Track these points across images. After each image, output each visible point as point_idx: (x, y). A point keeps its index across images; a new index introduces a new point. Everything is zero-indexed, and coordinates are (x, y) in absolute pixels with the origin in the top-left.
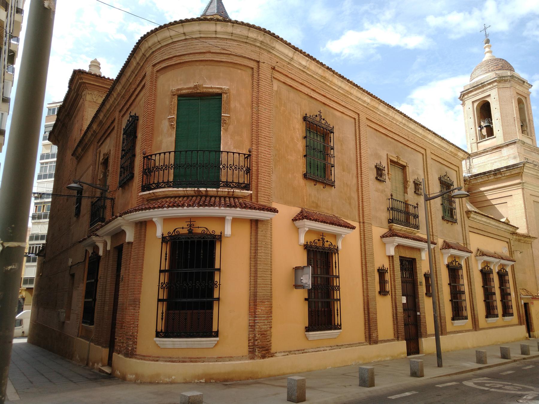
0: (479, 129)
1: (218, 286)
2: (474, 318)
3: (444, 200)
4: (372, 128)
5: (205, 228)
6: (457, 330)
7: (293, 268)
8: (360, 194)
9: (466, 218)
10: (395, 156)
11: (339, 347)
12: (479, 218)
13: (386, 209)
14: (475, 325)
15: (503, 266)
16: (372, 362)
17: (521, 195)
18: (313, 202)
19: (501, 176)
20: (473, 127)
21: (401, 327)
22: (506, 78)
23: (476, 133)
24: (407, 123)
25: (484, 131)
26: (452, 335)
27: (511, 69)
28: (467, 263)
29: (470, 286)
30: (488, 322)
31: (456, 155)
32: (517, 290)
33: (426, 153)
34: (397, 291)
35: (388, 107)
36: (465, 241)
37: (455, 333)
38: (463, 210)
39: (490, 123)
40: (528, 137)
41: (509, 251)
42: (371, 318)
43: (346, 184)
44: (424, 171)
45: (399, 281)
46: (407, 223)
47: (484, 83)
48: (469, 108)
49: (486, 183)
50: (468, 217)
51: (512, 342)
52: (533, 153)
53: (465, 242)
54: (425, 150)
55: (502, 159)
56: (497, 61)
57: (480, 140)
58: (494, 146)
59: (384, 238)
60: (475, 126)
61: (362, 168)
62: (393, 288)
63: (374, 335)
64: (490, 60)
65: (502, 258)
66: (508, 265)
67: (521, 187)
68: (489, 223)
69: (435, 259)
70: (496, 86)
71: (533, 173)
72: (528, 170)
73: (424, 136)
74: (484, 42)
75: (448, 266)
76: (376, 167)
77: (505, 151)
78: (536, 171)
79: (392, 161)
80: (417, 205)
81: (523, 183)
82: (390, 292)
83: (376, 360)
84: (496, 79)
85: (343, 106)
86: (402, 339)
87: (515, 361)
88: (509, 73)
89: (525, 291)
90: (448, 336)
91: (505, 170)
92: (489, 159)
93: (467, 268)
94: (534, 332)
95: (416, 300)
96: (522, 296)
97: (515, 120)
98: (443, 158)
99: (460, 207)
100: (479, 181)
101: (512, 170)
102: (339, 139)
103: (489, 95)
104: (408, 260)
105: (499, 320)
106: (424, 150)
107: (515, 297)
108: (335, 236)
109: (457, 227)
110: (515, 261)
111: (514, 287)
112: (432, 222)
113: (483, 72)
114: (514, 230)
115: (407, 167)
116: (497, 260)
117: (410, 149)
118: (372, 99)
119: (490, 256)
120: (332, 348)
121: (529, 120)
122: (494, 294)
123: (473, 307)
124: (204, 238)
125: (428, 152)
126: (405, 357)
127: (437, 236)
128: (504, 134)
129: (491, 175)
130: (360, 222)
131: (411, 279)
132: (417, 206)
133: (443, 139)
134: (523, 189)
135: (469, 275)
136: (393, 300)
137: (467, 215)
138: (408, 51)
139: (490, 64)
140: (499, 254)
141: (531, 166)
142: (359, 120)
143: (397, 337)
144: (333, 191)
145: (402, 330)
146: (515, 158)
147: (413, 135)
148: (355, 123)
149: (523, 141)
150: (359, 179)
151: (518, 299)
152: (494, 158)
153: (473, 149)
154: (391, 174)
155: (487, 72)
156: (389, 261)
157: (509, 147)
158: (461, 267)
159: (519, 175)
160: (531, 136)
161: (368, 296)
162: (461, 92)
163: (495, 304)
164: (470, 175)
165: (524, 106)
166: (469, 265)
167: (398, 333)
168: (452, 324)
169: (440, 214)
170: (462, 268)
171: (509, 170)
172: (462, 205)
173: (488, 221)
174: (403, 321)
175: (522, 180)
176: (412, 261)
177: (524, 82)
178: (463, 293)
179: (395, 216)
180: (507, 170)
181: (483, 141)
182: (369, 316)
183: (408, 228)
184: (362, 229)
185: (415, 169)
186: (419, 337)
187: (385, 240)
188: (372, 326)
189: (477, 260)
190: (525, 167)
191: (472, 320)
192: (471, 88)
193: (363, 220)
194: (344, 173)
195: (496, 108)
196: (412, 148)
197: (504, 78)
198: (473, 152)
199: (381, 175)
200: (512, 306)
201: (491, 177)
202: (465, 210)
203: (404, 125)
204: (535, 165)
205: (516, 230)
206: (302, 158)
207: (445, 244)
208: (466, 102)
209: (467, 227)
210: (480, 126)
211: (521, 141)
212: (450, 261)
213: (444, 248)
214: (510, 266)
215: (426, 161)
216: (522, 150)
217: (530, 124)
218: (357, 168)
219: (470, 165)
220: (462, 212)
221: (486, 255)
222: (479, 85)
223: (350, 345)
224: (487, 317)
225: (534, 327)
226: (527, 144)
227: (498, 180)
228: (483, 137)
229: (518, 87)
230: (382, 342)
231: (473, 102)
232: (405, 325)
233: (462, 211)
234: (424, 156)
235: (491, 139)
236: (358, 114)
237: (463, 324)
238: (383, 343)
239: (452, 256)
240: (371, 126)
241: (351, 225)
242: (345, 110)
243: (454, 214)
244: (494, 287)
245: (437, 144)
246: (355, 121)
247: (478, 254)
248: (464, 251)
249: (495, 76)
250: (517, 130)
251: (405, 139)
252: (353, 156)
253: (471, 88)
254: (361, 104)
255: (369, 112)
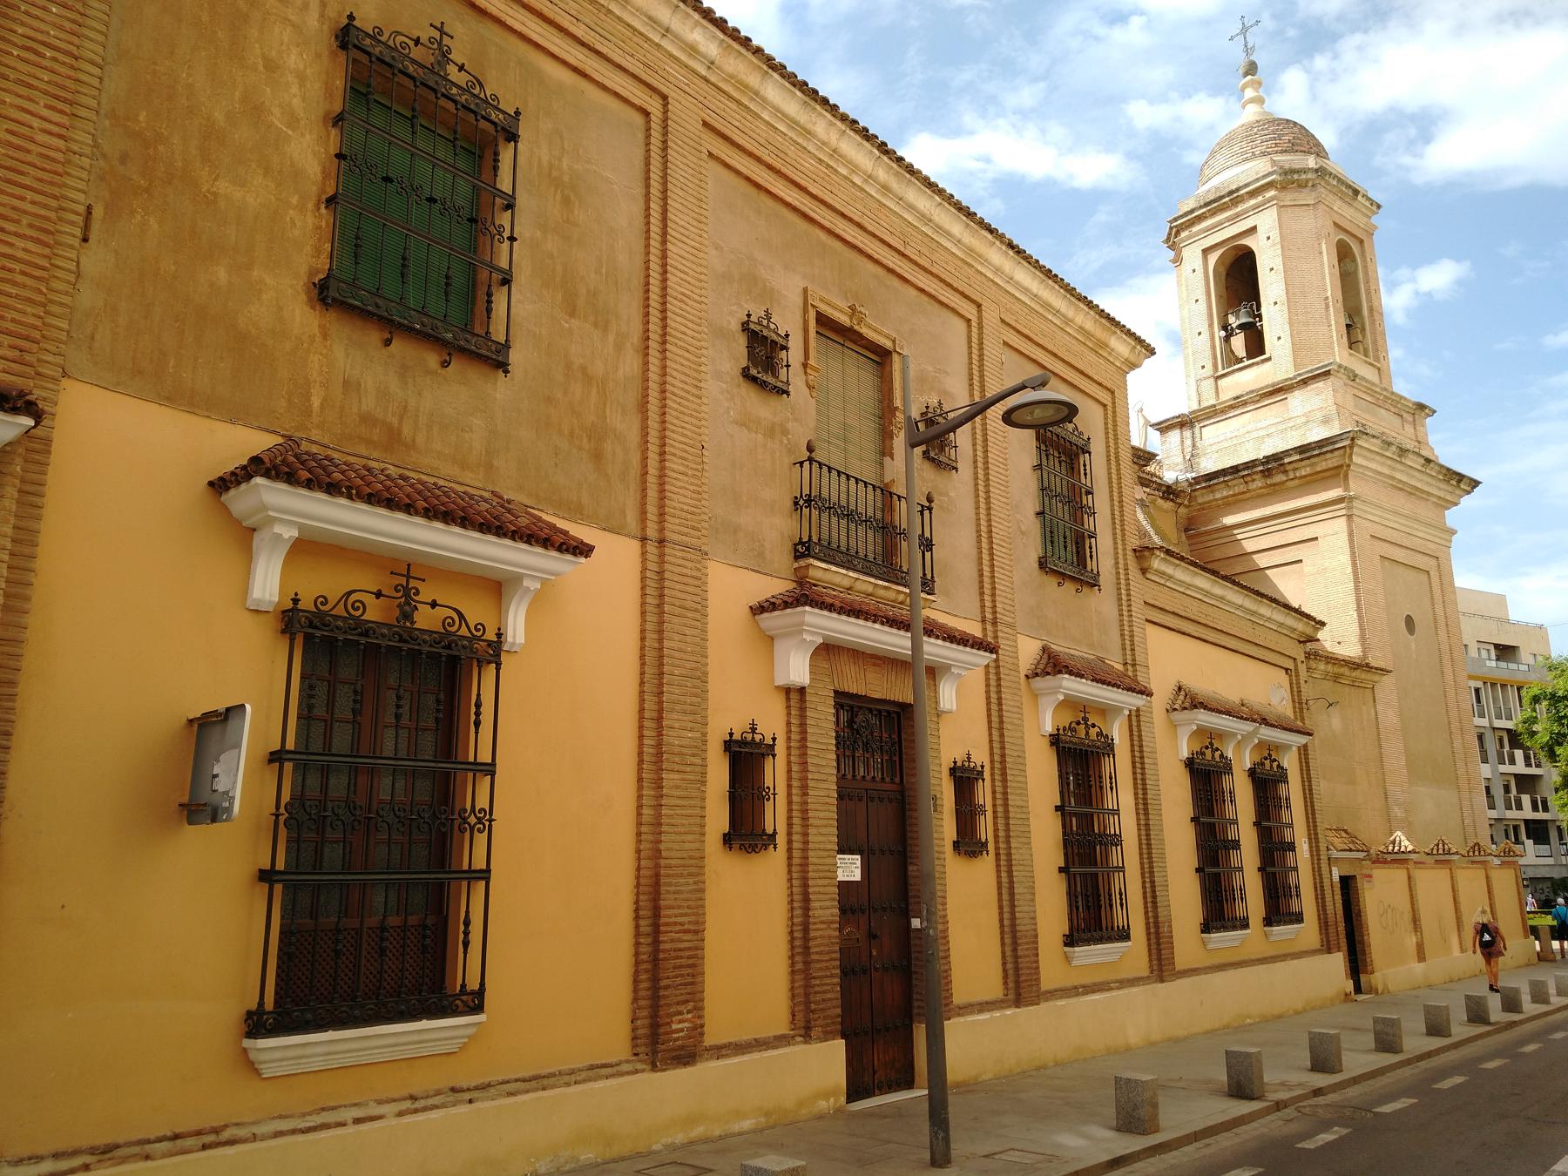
0: (1223, 333)
1: (772, 796)
2: (1157, 933)
3: (1050, 499)
4: (738, 173)
5: (455, 610)
6: (1088, 980)
7: (191, 721)
8: (653, 423)
9: (1134, 572)
10: (844, 305)
11: (467, 1096)
12: (1182, 574)
13: (789, 504)
14: (1159, 959)
15: (1269, 751)
16: (655, 1147)
17: (1345, 537)
18: (367, 419)
19: (1284, 478)
20: (1204, 328)
21: (828, 981)
22: (1304, 176)
23: (1213, 347)
24: (894, 184)
25: (1238, 343)
26: (1060, 1003)
27: (1317, 149)
28: (1135, 733)
29: (1142, 817)
30: (1210, 946)
31: (1104, 345)
32: (1316, 834)
33: (980, 318)
34: (811, 831)
35: (807, 99)
36: (1128, 652)
37: (1077, 995)
38: (1124, 545)
39: (1255, 317)
40: (1366, 362)
41: (1293, 701)
42: (665, 951)
43: (583, 369)
44: (971, 385)
45: (824, 788)
46: (887, 566)
47: (1238, 190)
48: (1194, 271)
49: (1240, 501)
50: (1144, 571)
51: (1297, 1013)
52: (1383, 411)
53: (1129, 657)
54: (979, 306)
55: (1290, 425)
56: (1278, 125)
57: (1223, 369)
58: (1266, 387)
59: (766, 615)
60: (1211, 326)
61: (669, 314)
62: (796, 821)
63: (674, 1026)
64: (1257, 122)
65: (1264, 721)
66: (1288, 747)
67: (1343, 512)
68: (1222, 598)
69: (1001, 710)
70: (1272, 199)
71: (1380, 469)
72: (1365, 458)
73: (970, 250)
74: (1241, 71)
75: (1055, 740)
76: (745, 327)
77: (1298, 402)
78: (1389, 462)
79: (822, 320)
80: (930, 500)
81: (1351, 499)
82: (991, 846)
83: (680, 1138)
84: (1274, 176)
85: (583, 44)
86: (826, 1033)
87: (1279, 1106)
88: (1311, 162)
89: (1344, 835)
90: (1044, 1006)
91: (1297, 457)
92: (1249, 428)
93: (1133, 751)
94: (1373, 972)
95: (911, 868)
96: (1335, 854)
97: (1327, 306)
98: (1050, 347)
99: (1114, 534)
100: (1218, 495)
101: (1316, 460)
102: (555, 174)
103: (1253, 230)
104: (880, 711)
105: (1253, 937)
106: (974, 307)
107: (1312, 856)
108: (497, 587)
109: (1102, 603)
110: (1310, 735)
111: (1308, 822)
112: (993, 571)
113: (1235, 160)
114: (1309, 631)
115: (895, 357)
116: (1248, 727)
117: (914, 293)
118: (730, 46)
119: (1220, 712)
120: (418, 1105)
121: (1371, 309)
122: (1236, 845)
123: (1154, 891)
124: (449, 647)
125: (991, 316)
126: (839, 1110)
127: (1011, 626)
128: (1296, 349)
129: (1254, 477)
130: (644, 539)
131: (888, 787)
132: (927, 504)
133: (1048, 273)
134: (1349, 517)
135: (1139, 776)
136: (794, 869)
137: (1139, 563)
138: (1076, 193)
139: (1256, 134)
140: (1257, 707)
141: (1374, 445)
142: (665, 120)
143: (805, 1027)
144: (500, 389)
145: (829, 996)
146: (1326, 421)
147: (926, 240)
148: (648, 129)
149: (1353, 371)
150: (654, 361)
151: (1319, 864)
152: (1263, 424)
153: (1205, 395)
154: (816, 370)
155: (1247, 159)
156: (788, 707)
157: (1309, 388)
158: (1109, 748)
159: (1338, 474)
160: (1377, 359)
161: (657, 854)
162: (1170, 222)
163: (1292, 881)
164: (1194, 475)
165: (1356, 269)
166: (1141, 740)
167: (808, 1011)
168: (1068, 959)
169: (1032, 549)
170: (1231, 768)
171: (1309, 458)
172: (1123, 525)
173: (1218, 591)
174: (837, 955)
175: (1347, 489)
176: (898, 714)
177: (1356, 192)
178: (1117, 840)
179: (834, 535)
180: (1302, 460)
181: (1233, 372)
182: (656, 942)
183: (880, 583)
184: (653, 566)
185: (931, 369)
186: (915, 1018)
187: (770, 620)
188: (667, 987)
189: (1174, 726)
190: (1355, 449)
191: (1149, 939)
192: (1201, 207)
193: (662, 530)
194: (575, 323)
195: (1272, 269)
196: (922, 290)
197: (1296, 177)
198: (1205, 404)
199: (770, 365)
200: (1297, 887)
201: (1254, 480)
202: (1133, 542)
203: (885, 188)
204: (1384, 442)
205: (1318, 629)
206: (310, 206)
207: (1046, 656)
208: (1186, 253)
209: (1137, 606)
210: (1225, 327)
211: (1346, 368)
212: (1065, 721)
213: (1039, 671)
214: (1294, 749)
215: (981, 349)
216: (1349, 397)
217: (1373, 322)
218: (647, 314)
219: (1194, 445)
220: (1120, 551)
221: (1205, 707)
222: (1223, 197)
223: (538, 1081)
224: (1206, 928)
225: (1374, 956)
226: (1363, 378)
227: (1275, 492)
228: (1231, 359)
229: (1338, 205)
230: (724, 1052)
231: (1206, 252)
232: (847, 972)
233: (1120, 546)
234: (975, 330)
235: (1257, 363)
236: (665, 98)
237: (1110, 959)
238: (727, 1056)
239: (1069, 703)
240: (728, 160)
241: (575, 539)
242: (590, 62)
243: (1088, 554)
244: (1235, 822)
245: (1026, 291)
246: (648, 121)
247: (1179, 702)
248: (1119, 687)
249: (1270, 170)
250: (1335, 338)
251: (890, 246)
252: (627, 257)
253: (1201, 207)
254: (676, 59)
255: (717, 102)
